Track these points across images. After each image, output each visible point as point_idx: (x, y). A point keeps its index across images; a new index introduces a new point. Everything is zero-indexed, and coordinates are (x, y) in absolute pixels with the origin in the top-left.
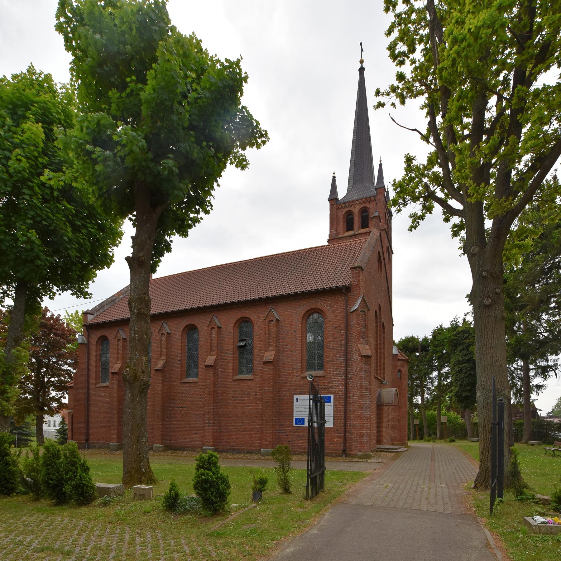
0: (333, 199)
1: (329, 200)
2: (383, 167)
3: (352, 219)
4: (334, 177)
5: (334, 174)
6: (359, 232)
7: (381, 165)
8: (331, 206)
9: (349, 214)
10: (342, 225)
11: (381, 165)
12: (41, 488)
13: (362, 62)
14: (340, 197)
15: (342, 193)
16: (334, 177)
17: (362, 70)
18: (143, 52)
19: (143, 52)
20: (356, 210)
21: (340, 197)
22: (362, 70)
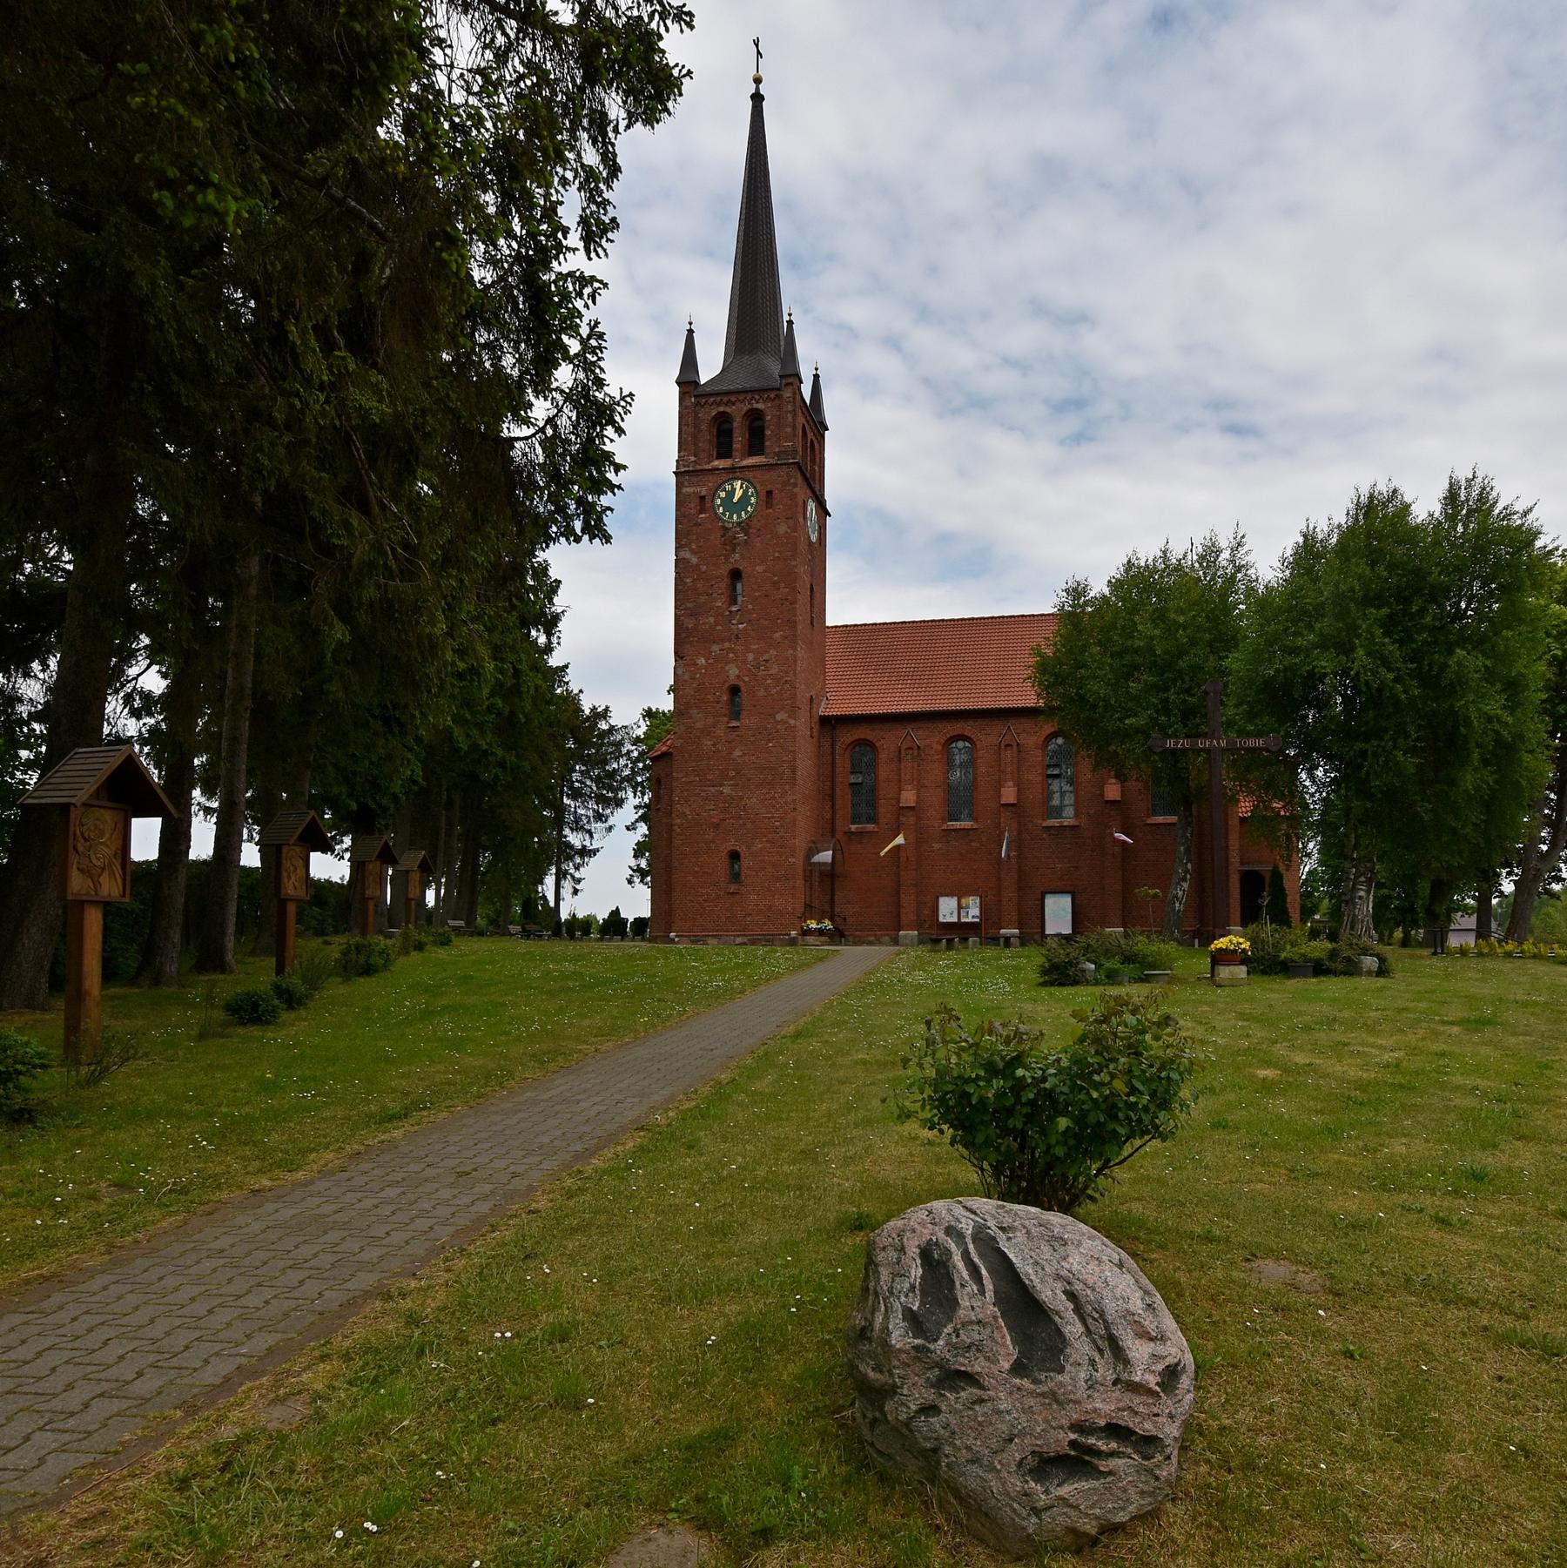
0: (687, 380)
1: (678, 383)
2: (821, 380)
3: (729, 433)
4: (691, 332)
5: (690, 323)
6: (745, 463)
7: (816, 377)
8: (683, 396)
9: (723, 421)
10: (707, 436)
11: (816, 377)
12: (240, 315)
13: (758, 81)
14: (704, 378)
15: (710, 365)
16: (691, 332)
17: (757, 98)
18: (264, 178)
19: (264, 178)
20: (738, 411)
21: (704, 378)
22: (757, 98)
